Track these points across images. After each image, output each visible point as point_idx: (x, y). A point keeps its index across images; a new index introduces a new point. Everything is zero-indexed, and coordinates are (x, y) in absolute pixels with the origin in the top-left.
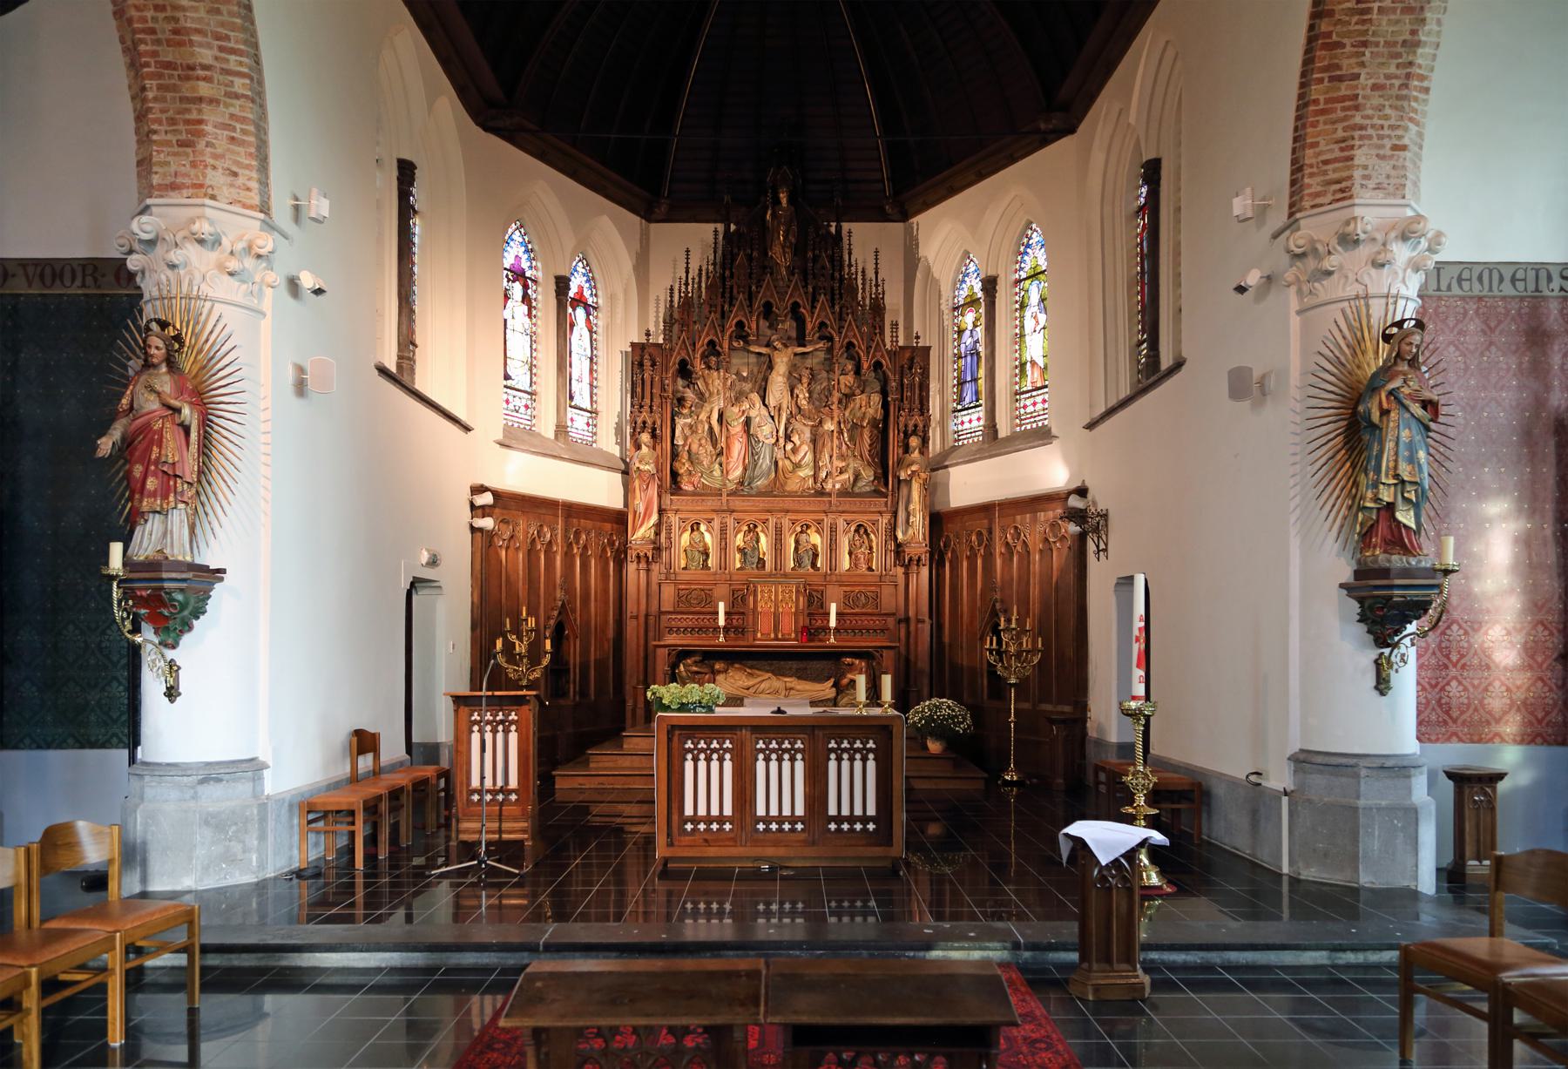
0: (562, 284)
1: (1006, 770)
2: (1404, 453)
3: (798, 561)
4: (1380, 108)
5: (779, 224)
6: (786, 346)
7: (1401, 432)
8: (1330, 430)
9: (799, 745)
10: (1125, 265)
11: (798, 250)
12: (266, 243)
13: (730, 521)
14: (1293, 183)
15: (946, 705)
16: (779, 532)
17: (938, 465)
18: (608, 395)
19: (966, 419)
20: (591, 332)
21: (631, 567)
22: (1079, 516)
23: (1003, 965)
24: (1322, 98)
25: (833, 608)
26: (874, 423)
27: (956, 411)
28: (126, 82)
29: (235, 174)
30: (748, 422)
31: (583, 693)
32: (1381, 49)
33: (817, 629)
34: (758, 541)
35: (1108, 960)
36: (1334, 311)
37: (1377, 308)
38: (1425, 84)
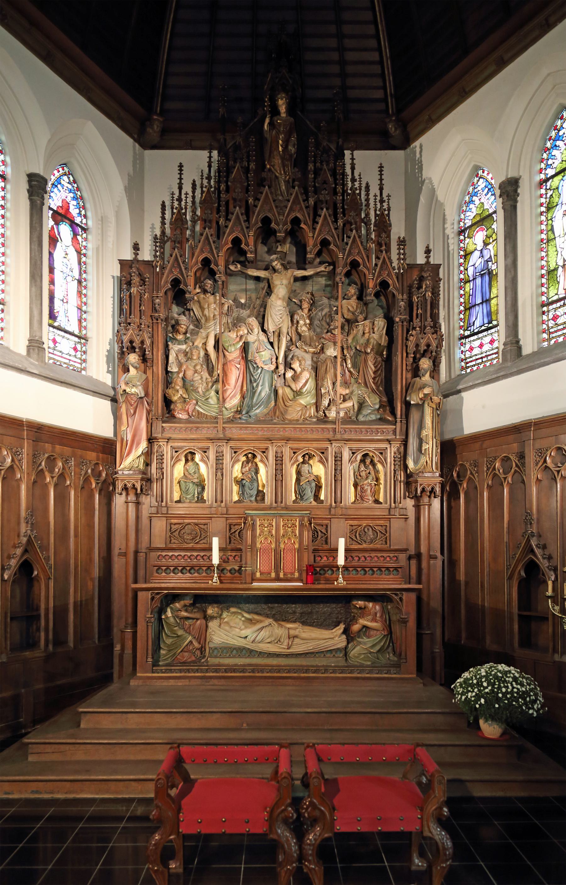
5: (278, 133)
6: (286, 268)
16: (279, 461)
17: (452, 391)
21: (119, 501)
25: (342, 544)
27: (463, 337)
30: (245, 348)
31: (59, 640)
33: (322, 568)
34: (257, 471)
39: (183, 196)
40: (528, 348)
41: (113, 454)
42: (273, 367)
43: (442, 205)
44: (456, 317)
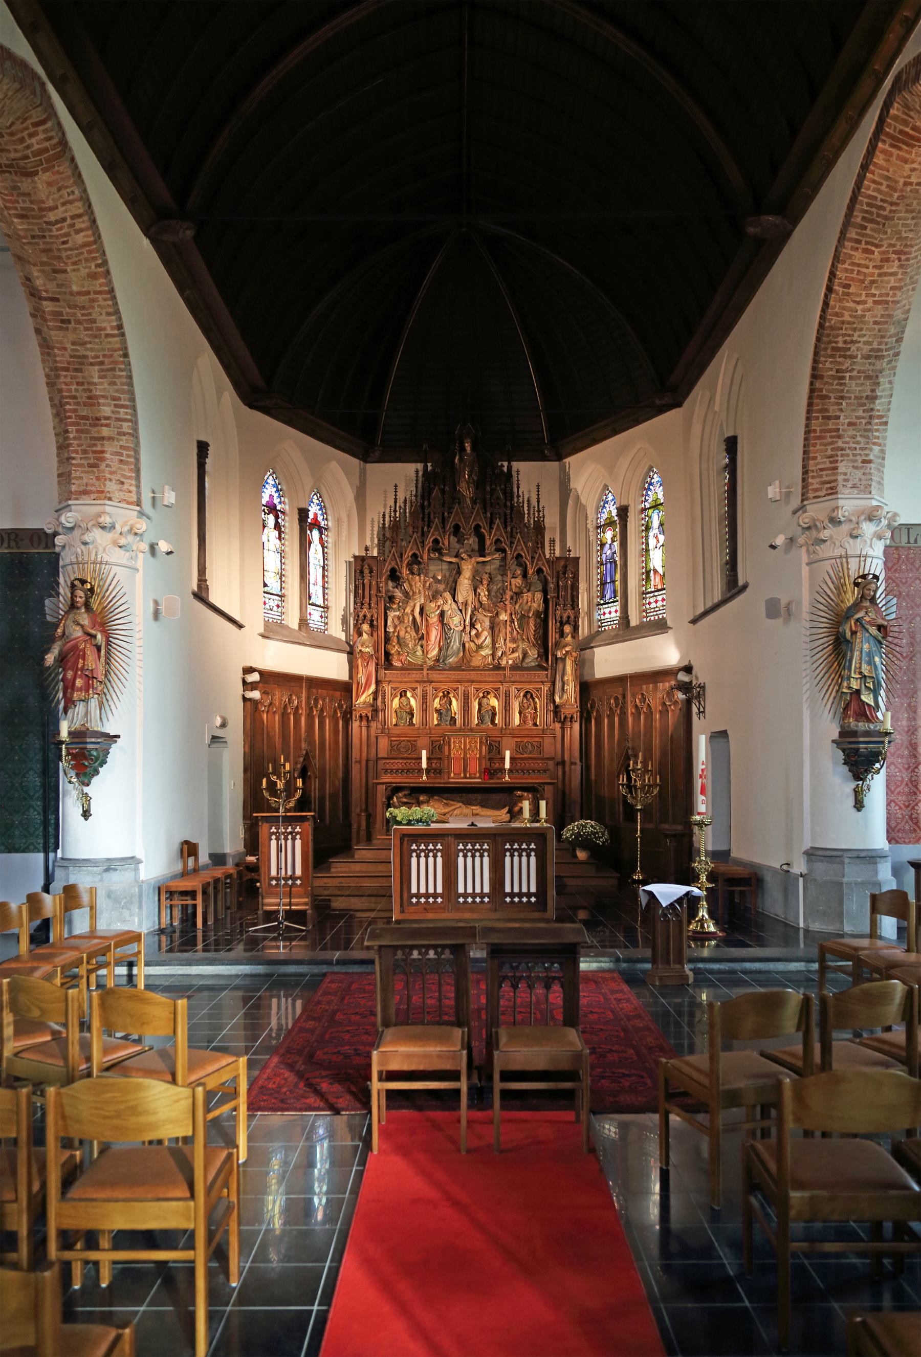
0: (303, 513)
1: (634, 871)
2: (865, 658)
3: (481, 719)
4: (854, 437)
6: (470, 557)
7: (863, 645)
8: (825, 641)
9: (486, 846)
10: (717, 507)
11: (479, 485)
12: (142, 526)
13: (430, 689)
14: (804, 480)
15: (590, 825)
17: (586, 646)
19: (607, 611)
20: (323, 547)
21: (356, 724)
22: (686, 687)
23: (610, 971)
24: (818, 429)
26: (537, 614)
27: (599, 604)
28: (52, 424)
29: (122, 483)
30: (442, 615)
32: (852, 401)
33: (495, 771)
34: (450, 703)
35: (668, 962)
36: (827, 566)
37: (853, 564)
38: (884, 420)
39: (398, 509)
40: (634, 622)
41: (350, 691)
42: (462, 628)
43: (585, 507)
44: (595, 589)
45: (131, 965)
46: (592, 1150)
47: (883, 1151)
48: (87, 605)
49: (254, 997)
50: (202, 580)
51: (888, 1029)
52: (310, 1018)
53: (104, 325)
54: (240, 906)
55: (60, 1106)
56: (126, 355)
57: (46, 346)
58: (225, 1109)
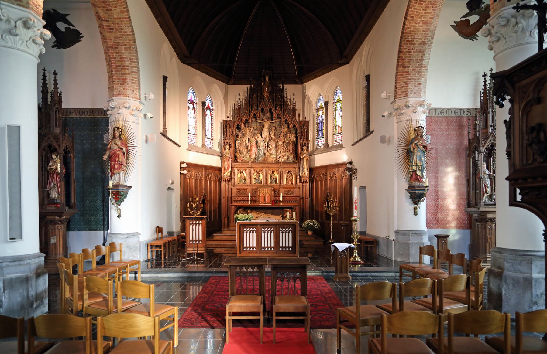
0: (204, 104)
1: (330, 239)
2: (418, 158)
3: (271, 181)
4: (415, 74)
7: (417, 153)
8: (403, 152)
9: (272, 229)
11: (271, 93)
12: (141, 107)
13: (252, 170)
14: (395, 91)
15: (313, 222)
16: (266, 174)
17: (312, 154)
18: (217, 135)
21: (223, 183)
22: (350, 170)
23: (320, 276)
25: (281, 195)
26: (293, 142)
30: (257, 142)
35: (342, 273)
40: (330, 145)
45: (136, 273)
46: (311, 342)
47: (424, 343)
48: (120, 137)
49: (183, 286)
50: (164, 128)
51: (426, 297)
52: (204, 293)
53: (126, 31)
54: (179, 251)
55: (103, 324)
56: (135, 42)
57: (104, 39)
58: (170, 326)
